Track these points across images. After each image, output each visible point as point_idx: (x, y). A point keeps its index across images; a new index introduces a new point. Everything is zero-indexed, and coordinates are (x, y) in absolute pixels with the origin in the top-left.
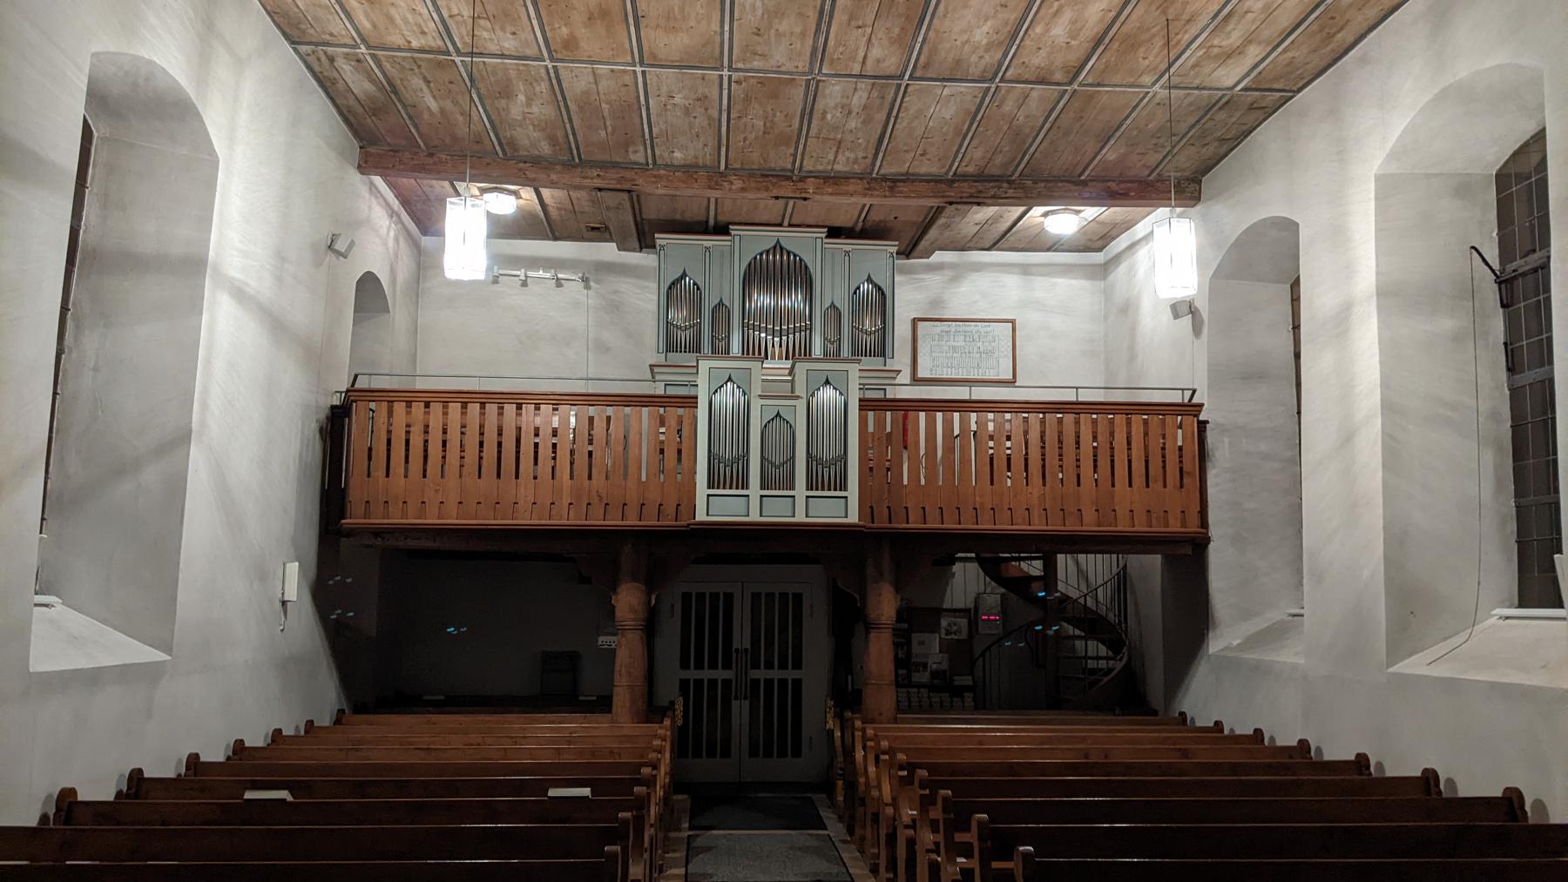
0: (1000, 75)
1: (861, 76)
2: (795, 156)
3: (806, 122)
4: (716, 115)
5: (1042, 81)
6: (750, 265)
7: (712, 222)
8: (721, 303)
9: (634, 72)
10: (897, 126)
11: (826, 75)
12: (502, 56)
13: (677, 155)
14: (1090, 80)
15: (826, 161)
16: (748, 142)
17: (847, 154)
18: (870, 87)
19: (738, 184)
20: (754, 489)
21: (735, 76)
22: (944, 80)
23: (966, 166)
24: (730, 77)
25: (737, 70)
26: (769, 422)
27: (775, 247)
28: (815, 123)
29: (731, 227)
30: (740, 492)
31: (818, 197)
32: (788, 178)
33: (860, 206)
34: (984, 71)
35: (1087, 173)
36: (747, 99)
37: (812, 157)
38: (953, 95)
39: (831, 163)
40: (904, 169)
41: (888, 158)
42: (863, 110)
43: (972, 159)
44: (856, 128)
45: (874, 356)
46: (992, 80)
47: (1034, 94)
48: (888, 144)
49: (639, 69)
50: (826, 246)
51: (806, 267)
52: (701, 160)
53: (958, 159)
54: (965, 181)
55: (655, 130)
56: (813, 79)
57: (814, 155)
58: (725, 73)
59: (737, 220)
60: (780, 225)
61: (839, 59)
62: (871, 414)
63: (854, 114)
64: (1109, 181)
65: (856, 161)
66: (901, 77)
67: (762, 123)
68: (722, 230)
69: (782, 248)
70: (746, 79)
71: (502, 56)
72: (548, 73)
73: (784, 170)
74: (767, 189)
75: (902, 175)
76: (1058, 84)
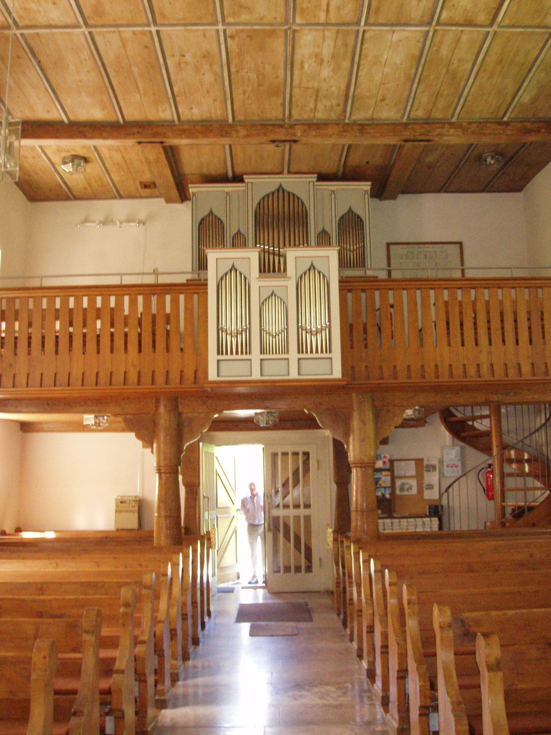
0: (436, 17)
1: (327, 24)
2: (283, 105)
3: (289, 73)
4: (218, 70)
5: (469, 23)
6: (259, 204)
7: (230, 174)
8: (239, 233)
9: (150, 32)
10: (360, 73)
11: (299, 25)
12: (51, 26)
13: (195, 111)
14: (507, 22)
15: (308, 109)
16: (247, 95)
17: (325, 102)
18: (335, 35)
19: (243, 132)
20: (256, 355)
21: (230, 30)
22: (392, 25)
23: (417, 110)
24: (225, 31)
25: (229, 24)
26: (266, 300)
27: (278, 190)
28: (296, 72)
29: (245, 177)
30: (245, 357)
31: (304, 140)
32: (281, 126)
33: (340, 147)
34: (423, 16)
35: (508, 114)
36: (240, 54)
37: (298, 106)
38: (401, 41)
39: (313, 111)
40: (369, 115)
41: (357, 105)
42: (332, 58)
43: (420, 103)
44: (328, 77)
45: (357, 267)
46: (430, 23)
47: (464, 38)
48: (354, 91)
49: (153, 29)
50: (318, 187)
51: (302, 203)
52: (214, 114)
53: (410, 103)
54: (416, 124)
55: (176, 89)
56: (290, 28)
57: (300, 104)
58: (221, 27)
59: (249, 170)
60: (281, 173)
61: (308, 8)
62: (350, 295)
63: (325, 63)
64: (525, 121)
65: (331, 108)
66: (358, 23)
67: (255, 76)
68: (238, 179)
69: (283, 191)
70: (238, 31)
71: (51, 26)
72: (86, 38)
73: (277, 119)
74: (265, 134)
75: (369, 120)
76: (481, 26)
